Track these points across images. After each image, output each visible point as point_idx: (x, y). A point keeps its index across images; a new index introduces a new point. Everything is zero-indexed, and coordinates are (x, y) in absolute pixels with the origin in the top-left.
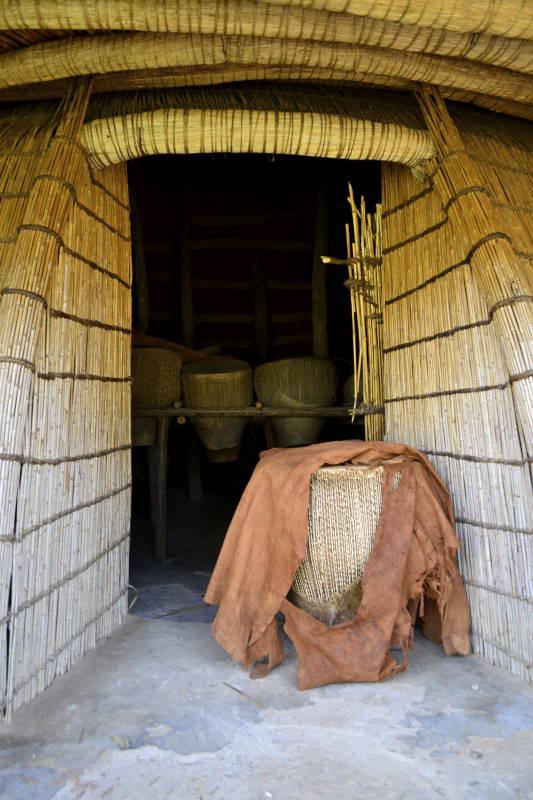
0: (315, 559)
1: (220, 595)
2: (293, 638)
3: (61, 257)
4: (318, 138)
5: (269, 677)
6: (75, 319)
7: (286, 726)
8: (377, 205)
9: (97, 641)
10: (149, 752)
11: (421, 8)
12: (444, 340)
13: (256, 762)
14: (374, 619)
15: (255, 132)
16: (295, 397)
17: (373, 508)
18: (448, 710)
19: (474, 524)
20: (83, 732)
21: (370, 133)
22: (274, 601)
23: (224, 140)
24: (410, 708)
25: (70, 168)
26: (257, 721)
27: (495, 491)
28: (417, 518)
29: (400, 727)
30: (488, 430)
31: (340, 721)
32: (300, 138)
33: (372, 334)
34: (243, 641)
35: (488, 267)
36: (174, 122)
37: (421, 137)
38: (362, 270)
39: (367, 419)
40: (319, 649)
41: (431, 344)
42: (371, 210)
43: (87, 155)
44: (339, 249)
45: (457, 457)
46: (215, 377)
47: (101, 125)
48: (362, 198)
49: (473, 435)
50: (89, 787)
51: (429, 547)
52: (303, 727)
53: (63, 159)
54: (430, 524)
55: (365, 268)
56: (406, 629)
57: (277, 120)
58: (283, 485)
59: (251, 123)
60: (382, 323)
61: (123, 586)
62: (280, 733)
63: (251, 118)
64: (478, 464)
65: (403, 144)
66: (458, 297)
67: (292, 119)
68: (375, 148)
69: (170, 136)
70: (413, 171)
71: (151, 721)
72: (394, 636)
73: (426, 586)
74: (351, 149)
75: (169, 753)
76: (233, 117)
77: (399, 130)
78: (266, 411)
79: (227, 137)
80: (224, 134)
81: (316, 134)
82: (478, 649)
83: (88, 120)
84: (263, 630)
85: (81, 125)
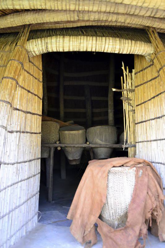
1: (73, 216)
2: (101, 233)
4: (112, 46)
8: (133, 70)
9: (26, 233)
14: (132, 227)
15: (88, 44)
23: (77, 47)
25: (21, 56)
28: (149, 187)
32: (105, 46)
36: (59, 41)
38: (127, 93)
39: (129, 149)
40: (111, 238)
42: (131, 72)
43: (28, 52)
44: (119, 86)
47: (33, 41)
48: (127, 67)
54: (154, 190)
55: (128, 93)
56: (145, 231)
59: (87, 41)
63: (87, 39)
67: (102, 39)
69: (58, 45)
72: (140, 234)
73: (152, 214)
76: (81, 39)
79: (78, 46)
81: (110, 45)
83: (28, 40)
84: (89, 230)
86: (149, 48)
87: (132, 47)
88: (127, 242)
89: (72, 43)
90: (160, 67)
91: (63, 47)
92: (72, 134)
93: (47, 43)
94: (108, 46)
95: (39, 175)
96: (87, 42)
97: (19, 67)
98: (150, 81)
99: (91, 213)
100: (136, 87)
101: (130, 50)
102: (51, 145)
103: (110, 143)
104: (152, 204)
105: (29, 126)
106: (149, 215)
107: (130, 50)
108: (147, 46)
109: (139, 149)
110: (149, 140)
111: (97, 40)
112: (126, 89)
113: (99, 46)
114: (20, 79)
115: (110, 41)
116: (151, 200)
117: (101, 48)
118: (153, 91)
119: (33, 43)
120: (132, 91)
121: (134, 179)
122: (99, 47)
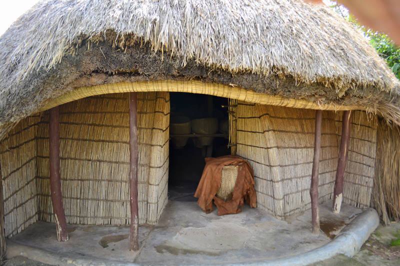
0: (222, 187)
1: (199, 195)
2: (217, 205)
14: (235, 200)
18: (251, 219)
19: (258, 178)
26: (211, 222)
28: (246, 178)
30: (262, 157)
31: (228, 221)
33: (234, 125)
39: (232, 148)
40: (223, 207)
41: (250, 133)
45: (255, 162)
51: (248, 184)
54: (248, 178)
56: (242, 202)
58: (215, 170)
72: (240, 203)
73: (247, 192)
78: (197, 135)
82: (258, 206)
99: (211, 192)
102: (134, 117)
106: (245, 193)
110: (246, 144)
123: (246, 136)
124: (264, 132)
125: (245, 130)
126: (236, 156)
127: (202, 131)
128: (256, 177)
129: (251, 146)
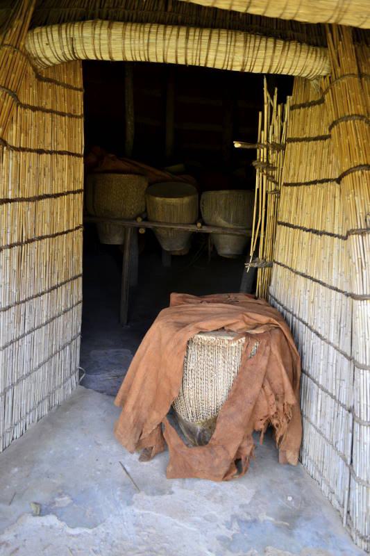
3: (4, 155)
4: (223, 55)
5: (152, 461)
6: (22, 200)
7: (146, 512)
8: (288, 97)
9: (50, 408)
10: (51, 520)
11: (265, 4)
12: (315, 236)
13: (117, 541)
15: (168, 47)
16: (228, 221)
17: (233, 369)
18: (263, 517)
20: (15, 494)
21: (271, 51)
22: (159, 415)
23: (142, 53)
24: (237, 510)
25: (13, 75)
27: (330, 367)
28: (266, 376)
29: (224, 527)
30: (332, 320)
32: (207, 55)
34: (135, 437)
35: (351, 196)
36: (100, 34)
37: (319, 55)
38: (268, 154)
39: (259, 271)
42: (282, 101)
43: (28, 57)
44: (252, 137)
45: (310, 328)
46: (169, 200)
47: (41, 32)
48: (276, 89)
49: (323, 319)
50: (5, 545)
52: (158, 514)
53: (8, 68)
55: (270, 152)
57: (187, 38)
58: (167, 343)
59: (164, 40)
60: (279, 197)
61: (73, 368)
62: (141, 517)
63: (164, 34)
64: (323, 342)
65: (301, 63)
66: (329, 207)
67: (200, 36)
68: (275, 65)
69: (97, 47)
70: (311, 82)
71: (60, 491)
74: (253, 66)
75: (63, 524)
76: (150, 32)
77: (298, 49)
78: (205, 229)
79: (144, 51)
80: (141, 48)
81: (221, 52)
83: (32, 28)
84: (149, 432)
85: (26, 31)
86: (317, 63)
87: (275, 58)
88: (210, 467)
89: (129, 42)
90: (334, 119)
91: (110, 53)
92: (169, 205)
93: (72, 39)
94: (216, 55)
95: (80, 306)
96: (164, 43)
97: (5, 104)
98: (315, 139)
99: (152, 406)
100: (290, 140)
101: (271, 67)
103: (244, 227)
104: (268, 409)
105: (46, 225)
107: (271, 67)
108: (314, 56)
109: (276, 279)
111: (190, 38)
112: (265, 143)
113: (193, 53)
114: (10, 133)
115: (220, 42)
116: (268, 401)
117: (198, 58)
118: (315, 170)
119: (42, 39)
120: (280, 148)
121: (238, 360)
122: (192, 56)
123: (296, 243)
124: (349, 233)
125: (295, 224)
126: (268, 301)
127: (223, 223)
128: (308, 376)
129: (306, 276)
